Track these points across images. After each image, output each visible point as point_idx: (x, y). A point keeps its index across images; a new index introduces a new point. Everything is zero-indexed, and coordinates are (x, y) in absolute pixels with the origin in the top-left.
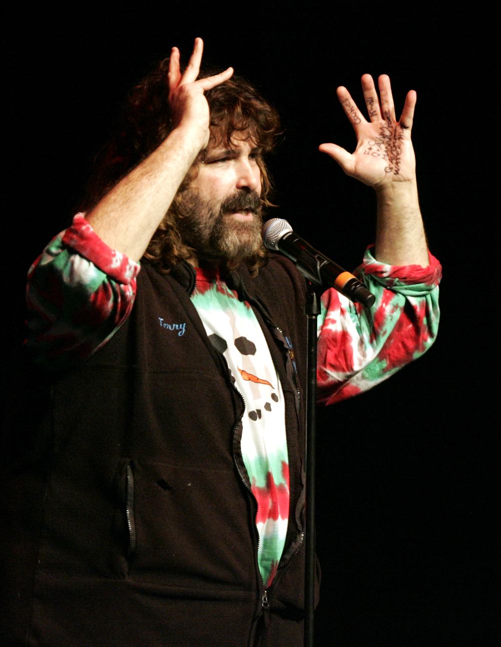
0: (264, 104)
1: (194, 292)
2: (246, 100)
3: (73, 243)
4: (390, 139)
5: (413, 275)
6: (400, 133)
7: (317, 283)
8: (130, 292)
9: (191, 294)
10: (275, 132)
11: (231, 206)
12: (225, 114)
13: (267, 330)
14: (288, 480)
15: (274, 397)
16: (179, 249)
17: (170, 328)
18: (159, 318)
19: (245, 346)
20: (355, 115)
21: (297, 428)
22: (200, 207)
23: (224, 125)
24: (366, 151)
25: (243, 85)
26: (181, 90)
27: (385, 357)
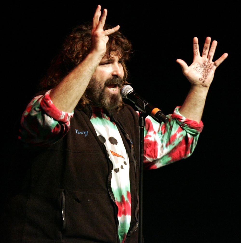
1: (92, 117)
2: (117, 38)
7: (143, 112)
10: (131, 51)
13: (122, 135)
15: (125, 163)
17: (81, 134)
18: (76, 130)
19: (113, 141)
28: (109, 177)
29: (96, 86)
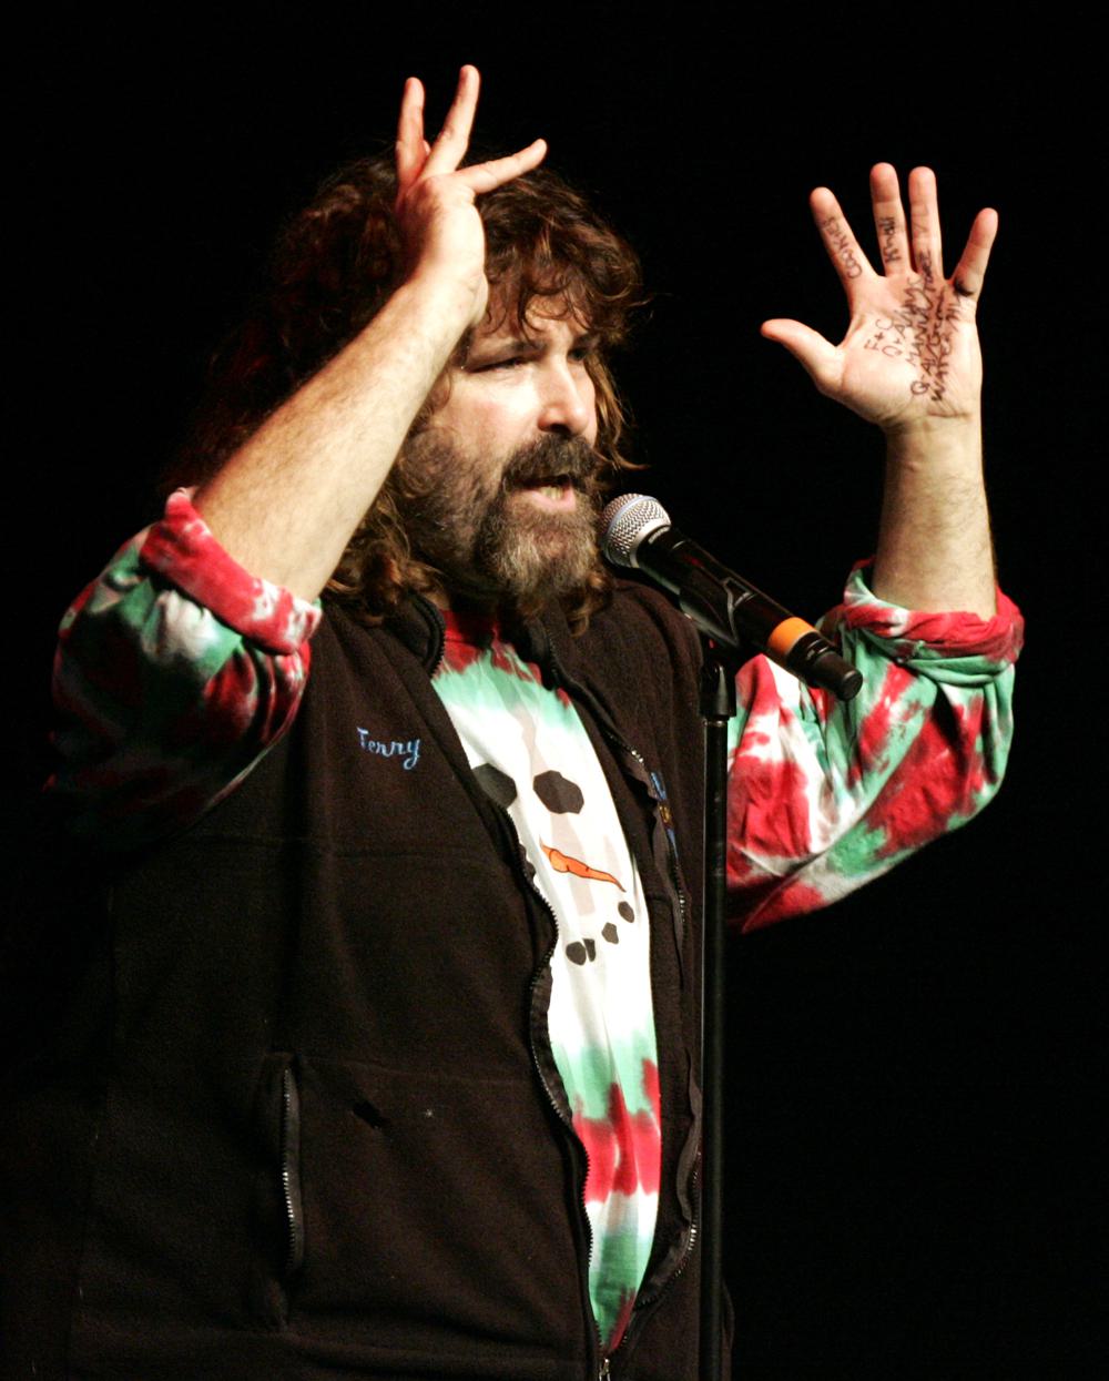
0: (603, 234)
1: (440, 667)
2: (561, 224)
3: (164, 564)
4: (927, 318)
5: (959, 636)
6: (951, 305)
7: (725, 642)
8: (296, 672)
9: (433, 672)
10: (631, 298)
11: (529, 471)
12: (511, 256)
14: (657, 1104)
15: (625, 910)
16: (404, 570)
17: (384, 752)
18: (359, 730)
19: (558, 794)
20: (850, 256)
21: (678, 982)
22: (455, 473)
23: (510, 280)
24: (869, 341)
25: (558, 190)
26: (423, 192)
27: (884, 823)
28: (539, 987)
29: (456, 485)
